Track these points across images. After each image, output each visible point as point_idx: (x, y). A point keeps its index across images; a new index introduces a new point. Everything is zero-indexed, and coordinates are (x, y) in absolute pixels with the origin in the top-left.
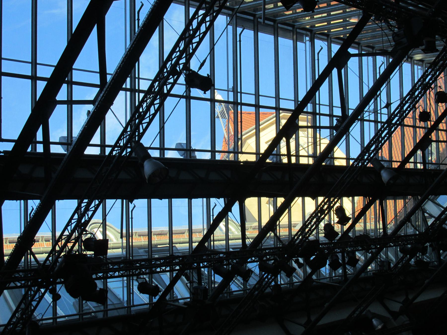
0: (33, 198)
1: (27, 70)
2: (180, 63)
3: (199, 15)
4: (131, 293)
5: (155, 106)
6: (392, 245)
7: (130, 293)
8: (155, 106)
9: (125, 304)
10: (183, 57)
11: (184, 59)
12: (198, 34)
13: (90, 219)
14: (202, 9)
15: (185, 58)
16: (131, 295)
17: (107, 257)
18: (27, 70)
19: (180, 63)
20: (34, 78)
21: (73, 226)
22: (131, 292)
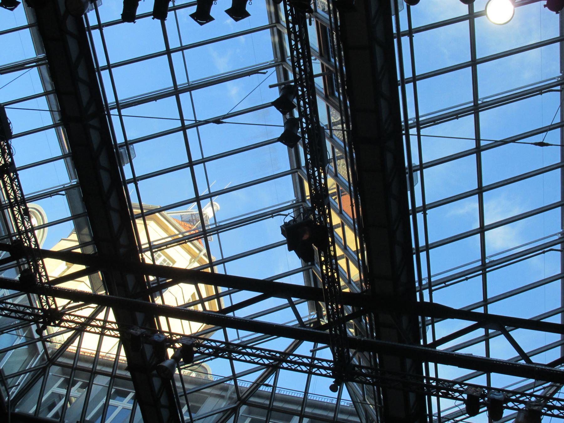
0: (120, 335)
1: (203, 192)
2: (462, 395)
3: (327, 373)
4: (445, 284)
5: (299, 367)
6: (369, 378)
7: (444, 282)
8: (299, 367)
9: (269, 391)
10: (515, 403)
11: (269, 362)
12: (516, 404)
13: (36, 241)
14: (227, 355)
15: (269, 362)
16: (443, 285)
17: (25, 197)
18: (203, 192)
19: (462, 395)
20: (486, 302)
21: (79, 321)
22: (447, 283)
